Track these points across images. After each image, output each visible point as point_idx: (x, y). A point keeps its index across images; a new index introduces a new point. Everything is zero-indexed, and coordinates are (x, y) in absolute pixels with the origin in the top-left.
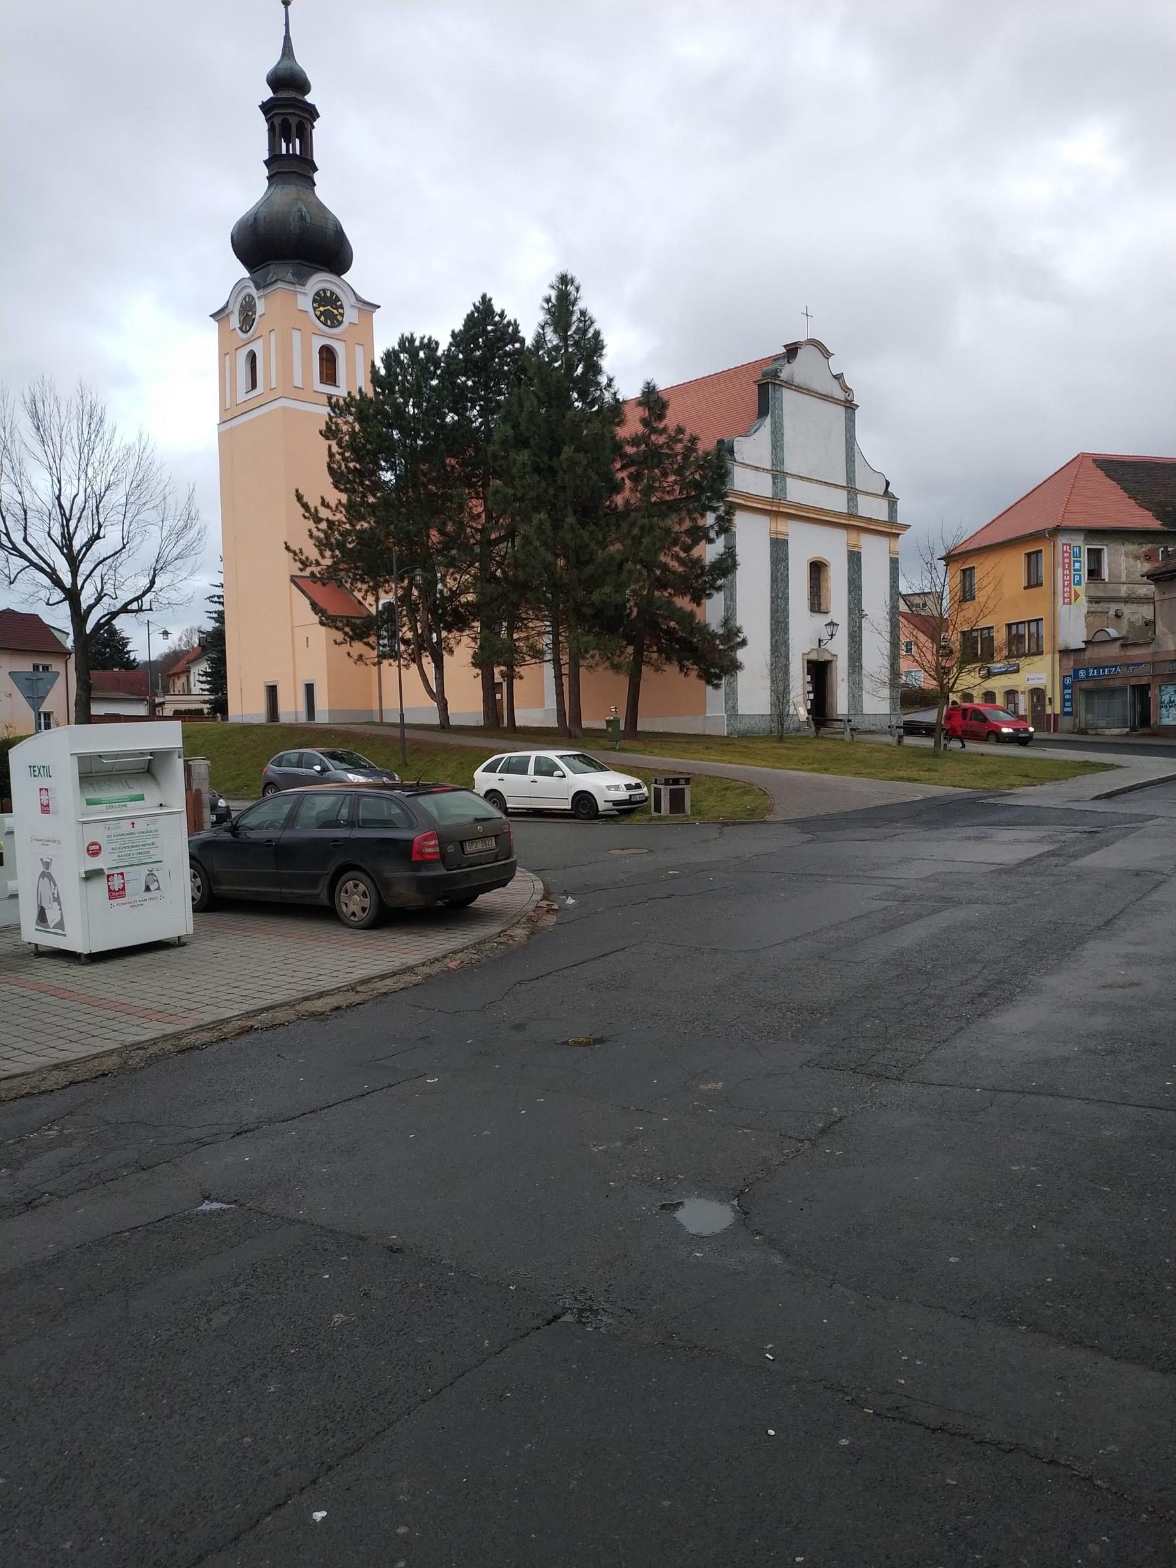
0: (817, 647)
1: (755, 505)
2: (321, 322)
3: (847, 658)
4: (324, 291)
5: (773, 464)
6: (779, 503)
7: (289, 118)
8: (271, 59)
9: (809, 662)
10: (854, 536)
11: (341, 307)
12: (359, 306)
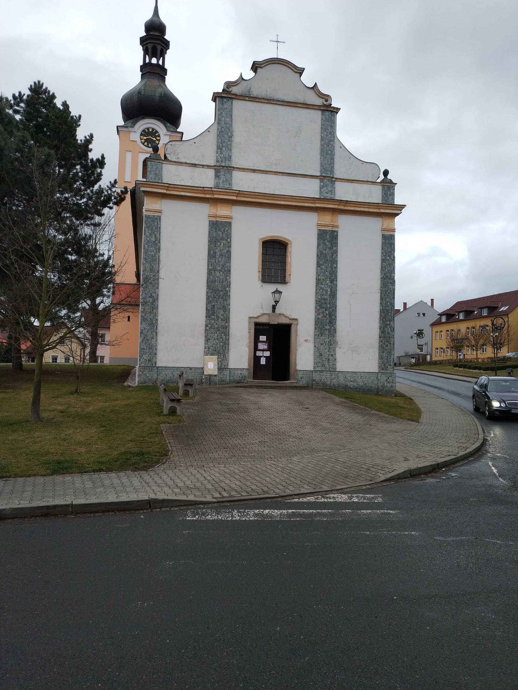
0: (270, 311)
1: (183, 194)
2: (145, 146)
3: (313, 323)
4: (148, 129)
5: (218, 161)
6: (212, 191)
7: (156, 45)
8: (148, 15)
9: (257, 324)
10: (327, 219)
11: (159, 136)
12: (170, 134)
